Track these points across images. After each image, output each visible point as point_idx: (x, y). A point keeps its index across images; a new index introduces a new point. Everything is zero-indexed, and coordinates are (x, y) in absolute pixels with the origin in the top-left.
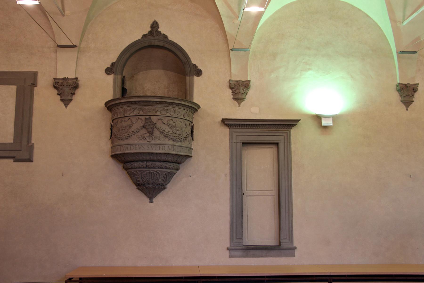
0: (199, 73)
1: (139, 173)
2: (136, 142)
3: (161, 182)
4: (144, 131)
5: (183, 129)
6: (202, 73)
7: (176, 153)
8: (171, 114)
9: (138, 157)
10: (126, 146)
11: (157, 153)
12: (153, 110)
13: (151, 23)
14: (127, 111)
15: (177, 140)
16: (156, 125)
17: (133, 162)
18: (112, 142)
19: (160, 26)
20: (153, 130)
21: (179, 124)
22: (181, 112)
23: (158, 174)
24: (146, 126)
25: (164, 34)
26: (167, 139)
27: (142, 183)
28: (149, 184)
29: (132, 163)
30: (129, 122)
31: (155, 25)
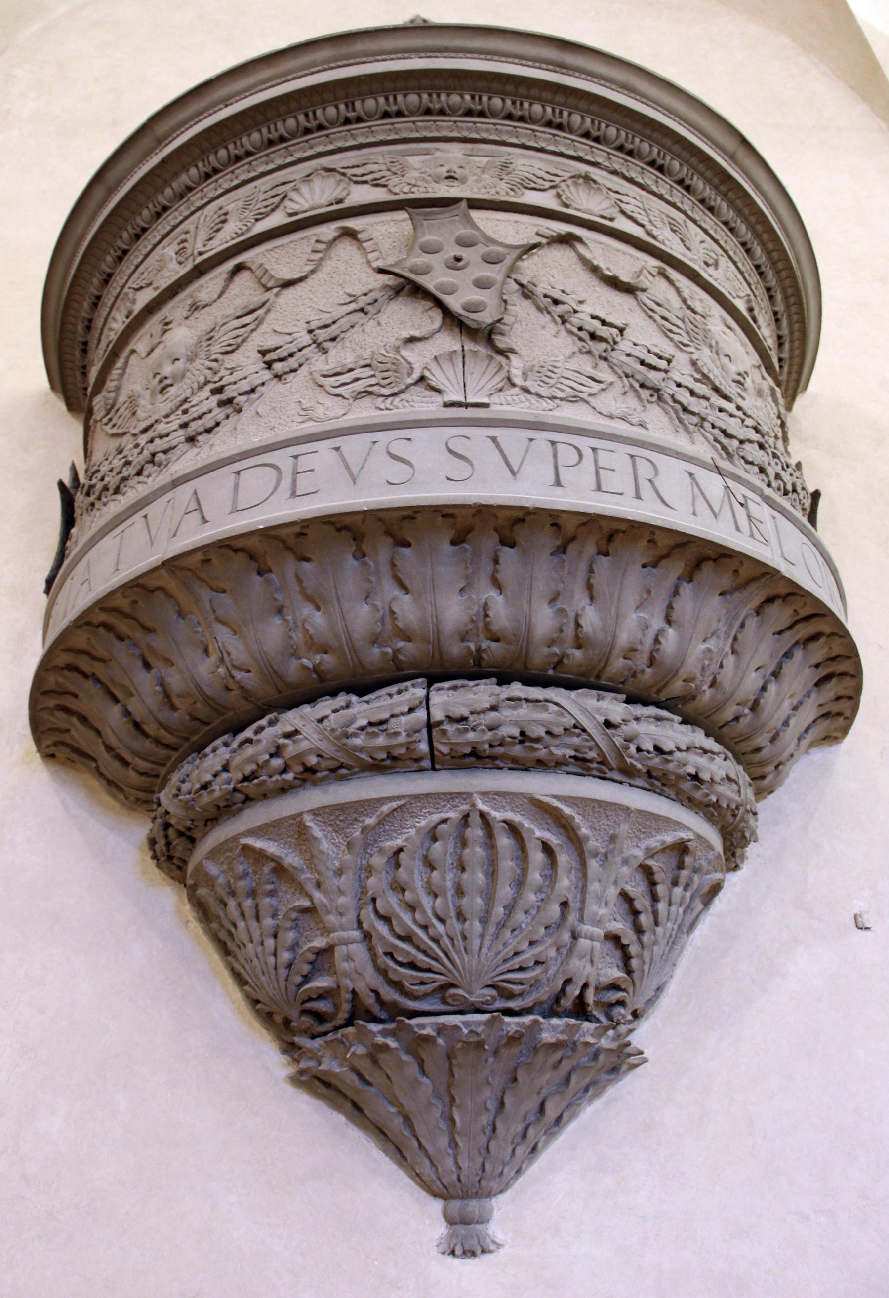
9: (318, 620)
23: (563, 858)
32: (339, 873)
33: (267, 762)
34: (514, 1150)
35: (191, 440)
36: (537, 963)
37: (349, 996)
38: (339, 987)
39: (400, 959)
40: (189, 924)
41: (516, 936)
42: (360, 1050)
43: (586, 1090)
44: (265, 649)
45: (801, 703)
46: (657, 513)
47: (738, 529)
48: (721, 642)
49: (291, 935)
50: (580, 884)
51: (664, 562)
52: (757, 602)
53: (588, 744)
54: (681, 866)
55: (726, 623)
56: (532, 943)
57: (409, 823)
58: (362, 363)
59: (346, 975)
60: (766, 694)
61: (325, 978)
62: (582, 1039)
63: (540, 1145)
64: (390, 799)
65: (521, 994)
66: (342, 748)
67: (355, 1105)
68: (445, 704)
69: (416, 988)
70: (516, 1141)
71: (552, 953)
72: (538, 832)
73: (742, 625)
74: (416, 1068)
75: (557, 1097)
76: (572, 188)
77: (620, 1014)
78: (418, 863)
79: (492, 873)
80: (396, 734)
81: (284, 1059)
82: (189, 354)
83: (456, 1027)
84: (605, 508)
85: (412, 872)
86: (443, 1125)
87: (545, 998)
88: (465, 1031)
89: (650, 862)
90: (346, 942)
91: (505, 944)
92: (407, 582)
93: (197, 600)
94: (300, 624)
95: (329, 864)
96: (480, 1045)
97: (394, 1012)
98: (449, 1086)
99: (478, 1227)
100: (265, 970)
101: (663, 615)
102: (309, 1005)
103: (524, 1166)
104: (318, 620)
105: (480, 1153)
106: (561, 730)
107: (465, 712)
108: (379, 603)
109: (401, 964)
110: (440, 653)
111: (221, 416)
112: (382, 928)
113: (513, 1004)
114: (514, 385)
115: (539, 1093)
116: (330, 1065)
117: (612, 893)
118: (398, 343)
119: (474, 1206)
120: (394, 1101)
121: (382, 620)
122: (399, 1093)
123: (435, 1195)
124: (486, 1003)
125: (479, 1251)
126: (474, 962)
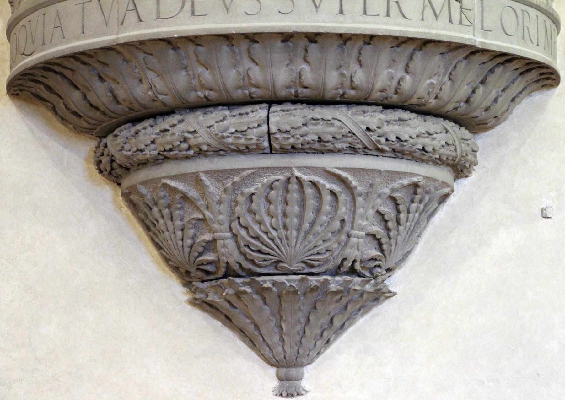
1: (212, 187)
3: (362, 250)
7: (479, 40)
9: (207, 76)
17: (169, 112)
23: (343, 197)
29: (164, 123)
32: (220, 202)
33: (178, 145)
34: (316, 343)
36: (326, 250)
37: (225, 265)
38: (219, 259)
39: (253, 249)
40: (122, 209)
41: (316, 237)
42: (231, 291)
43: (359, 310)
44: (177, 87)
45: (507, 87)
46: (398, 25)
47: (450, 21)
48: (441, 78)
49: (192, 232)
50: (353, 209)
51: (403, 45)
52: (465, 55)
53: (356, 141)
54: (415, 193)
55: (444, 67)
57: (258, 180)
59: (223, 255)
60: (474, 95)
61: (212, 254)
63: (331, 339)
64: (248, 169)
65: (319, 265)
66: (220, 143)
67: (227, 317)
68: (277, 123)
69: (261, 263)
70: (316, 338)
71: (335, 246)
72: (328, 185)
73: (455, 67)
74: (262, 302)
75: (340, 316)
77: (377, 272)
78: (263, 200)
79: (303, 205)
80: (251, 139)
81: (185, 290)
83: (283, 283)
84: (366, 29)
85: (260, 205)
86: (276, 330)
87: (331, 268)
88: (288, 284)
90: (224, 239)
92: (257, 61)
93: (136, 58)
94: (197, 76)
95: (214, 198)
96: (295, 292)
98: (280, 310)
99: (295, 382)
100: (176, 247)
101: (404, 69)
102: (201, 267)
103: (322, 351)
104: (207, 76)
105: (296, 344)
106: (341, 136)
107: (288, 128)
108: (241, 70)
109: (253, 251)
110: (275, 93)
112: (243, 233)
113: (314, 270)
115: (329, 314)
116: (213, 297)
117: (371, 212)
119: (293, 371)
120: (248, 316)
121: (243, 79)
122: (251, 313)
124: (300, 270)
125: (296, 394)
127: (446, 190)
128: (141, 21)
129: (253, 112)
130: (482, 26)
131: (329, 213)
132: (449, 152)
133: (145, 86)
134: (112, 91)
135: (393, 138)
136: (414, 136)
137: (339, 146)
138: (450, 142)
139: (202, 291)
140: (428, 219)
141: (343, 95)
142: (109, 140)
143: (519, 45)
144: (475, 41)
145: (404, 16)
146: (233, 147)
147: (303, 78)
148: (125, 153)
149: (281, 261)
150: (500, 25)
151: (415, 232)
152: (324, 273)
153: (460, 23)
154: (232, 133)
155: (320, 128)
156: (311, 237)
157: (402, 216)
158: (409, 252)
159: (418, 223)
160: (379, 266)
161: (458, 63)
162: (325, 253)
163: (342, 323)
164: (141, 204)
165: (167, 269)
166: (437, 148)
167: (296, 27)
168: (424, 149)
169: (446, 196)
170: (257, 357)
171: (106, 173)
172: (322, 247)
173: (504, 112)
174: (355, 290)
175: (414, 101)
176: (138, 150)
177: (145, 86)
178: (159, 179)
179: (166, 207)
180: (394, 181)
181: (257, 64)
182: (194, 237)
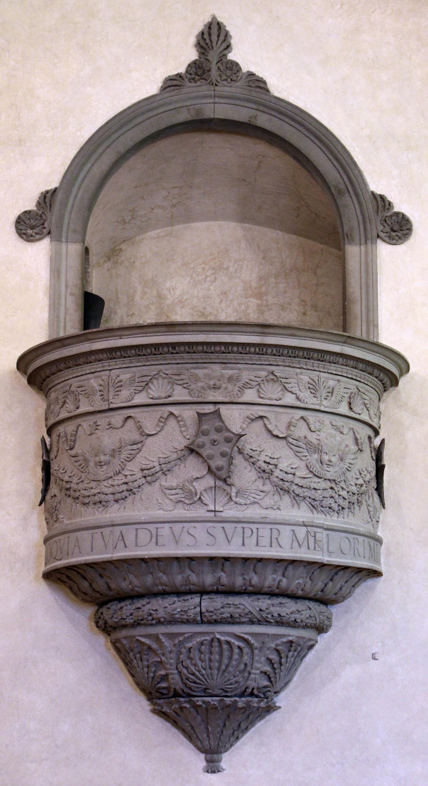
0: (399, 228)
1: (166, 642)
2: (159, 514)
4: (192, 468)
5: (349, 458)
6: (410, 229)
7: (326, 559)
8: (301, 395)
10: (117, 530)
11: (246, 560)
12: (230, 379)
13: (199, 27)
14: (119, 386)
15: (326, 502)
16: (240, 444)
17: (141, 596)
18: (51, 516)
19: (233, 42)
20: (230, 464)
21: (334, 437)
22: (338, 386)
24: (202, 446)
25: (251, 74)
26: (287, 499)
27: (179, 686)
28: (206, 692)
29: (139, 603)
30: (129, 433)
31: (214, 38)
32: (171, 652)
33: (147, 618)
35: (117, 501)
36: (236, 682)
37: (173, 690)
38: (170, 686)
42: (177, 706)
43: (257, 718)
46: (277, 552)
47: (309, 548)
49: (153, 669)
50: (252, 657)
54: (291, 646)
56: (234, 676)
57: (194, 639)
58: (179, 487)
60: (326, 588)
62: (253, 705)
63: (240, 736)
65: (231, 691)
71: (241, 679)
73: (313, 573)
74: (196, 713)
76: (266, 383)
78: (197, 651)
80: (190, 616)
81: (148, 703)
82: (111, 453)
84: (257, 555)
85: (195, 654)
86: (205, 730)
88: (212, 703)
89: (278, 648)
90: (172, 674)
91: (225, 677)
97: (189, 695)
99: (217, 764)
102: (159, 690)
106: (244, 614)
107: (212, 609)
109: (191, 682)
111: (127, 495)
112: (185, 671)
113: (228, 694)
114: (232, 500)
115: (238, 721)
116: (165, 709)
117: (263, 659)
118: (192, 480)
119: (215, 756)
120: (188, 722)
121: (186, 581)
123: (202, 752)
125: (217, 771)
126: (215, 683)
127: (312, 643)
128: (126, 547)
129: (191, 599)
130: (328, 550)
131: (238, 660)
132: (311, 621)
133: (127, 582)
134: (107, 584)
135: (276, 615)
136: (289, 613)
137: (243, 620)
138: (312, 615)
139: (159, 705)
140: (302, 660)
141: (245, 589)
142: (104, 609)
143: (351, 559)
144: (324, 560)
145: (280, 546)
146: (179, 620)
147: (221, 581)
148: (114, 620)
149: (207, 689)
150: (339, 548)
151: (293, 668)
152: (235, 696)
153: (315, 549)
154: (179, 612)
155: (232, 609)
156: (226, 674)
157: (283, 660)
158: (290, 681)
159: (294, 663)
160: (269, 691)
161: (314, 571)
162: (235, 684)
163: (246, 726)
164: (122, 649)
165: (138, 690)
166: (304, 620)
167: (216, 553)
168: (295, 620)
169: (311, 647)
170: (193, 747)
171: (101, 629)
172: (233, 681)
173: (348, 594)
174: (254, 707)
175: (289, 592)
176: (122, 618)
177: (127, 582)
178: (134, 636)
179: (138, 653)
180: (278, 639)
181: (194, 572)
182: (155, 672)
